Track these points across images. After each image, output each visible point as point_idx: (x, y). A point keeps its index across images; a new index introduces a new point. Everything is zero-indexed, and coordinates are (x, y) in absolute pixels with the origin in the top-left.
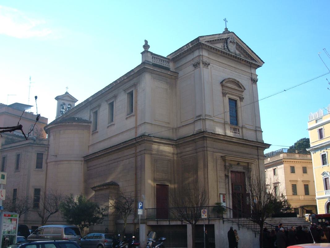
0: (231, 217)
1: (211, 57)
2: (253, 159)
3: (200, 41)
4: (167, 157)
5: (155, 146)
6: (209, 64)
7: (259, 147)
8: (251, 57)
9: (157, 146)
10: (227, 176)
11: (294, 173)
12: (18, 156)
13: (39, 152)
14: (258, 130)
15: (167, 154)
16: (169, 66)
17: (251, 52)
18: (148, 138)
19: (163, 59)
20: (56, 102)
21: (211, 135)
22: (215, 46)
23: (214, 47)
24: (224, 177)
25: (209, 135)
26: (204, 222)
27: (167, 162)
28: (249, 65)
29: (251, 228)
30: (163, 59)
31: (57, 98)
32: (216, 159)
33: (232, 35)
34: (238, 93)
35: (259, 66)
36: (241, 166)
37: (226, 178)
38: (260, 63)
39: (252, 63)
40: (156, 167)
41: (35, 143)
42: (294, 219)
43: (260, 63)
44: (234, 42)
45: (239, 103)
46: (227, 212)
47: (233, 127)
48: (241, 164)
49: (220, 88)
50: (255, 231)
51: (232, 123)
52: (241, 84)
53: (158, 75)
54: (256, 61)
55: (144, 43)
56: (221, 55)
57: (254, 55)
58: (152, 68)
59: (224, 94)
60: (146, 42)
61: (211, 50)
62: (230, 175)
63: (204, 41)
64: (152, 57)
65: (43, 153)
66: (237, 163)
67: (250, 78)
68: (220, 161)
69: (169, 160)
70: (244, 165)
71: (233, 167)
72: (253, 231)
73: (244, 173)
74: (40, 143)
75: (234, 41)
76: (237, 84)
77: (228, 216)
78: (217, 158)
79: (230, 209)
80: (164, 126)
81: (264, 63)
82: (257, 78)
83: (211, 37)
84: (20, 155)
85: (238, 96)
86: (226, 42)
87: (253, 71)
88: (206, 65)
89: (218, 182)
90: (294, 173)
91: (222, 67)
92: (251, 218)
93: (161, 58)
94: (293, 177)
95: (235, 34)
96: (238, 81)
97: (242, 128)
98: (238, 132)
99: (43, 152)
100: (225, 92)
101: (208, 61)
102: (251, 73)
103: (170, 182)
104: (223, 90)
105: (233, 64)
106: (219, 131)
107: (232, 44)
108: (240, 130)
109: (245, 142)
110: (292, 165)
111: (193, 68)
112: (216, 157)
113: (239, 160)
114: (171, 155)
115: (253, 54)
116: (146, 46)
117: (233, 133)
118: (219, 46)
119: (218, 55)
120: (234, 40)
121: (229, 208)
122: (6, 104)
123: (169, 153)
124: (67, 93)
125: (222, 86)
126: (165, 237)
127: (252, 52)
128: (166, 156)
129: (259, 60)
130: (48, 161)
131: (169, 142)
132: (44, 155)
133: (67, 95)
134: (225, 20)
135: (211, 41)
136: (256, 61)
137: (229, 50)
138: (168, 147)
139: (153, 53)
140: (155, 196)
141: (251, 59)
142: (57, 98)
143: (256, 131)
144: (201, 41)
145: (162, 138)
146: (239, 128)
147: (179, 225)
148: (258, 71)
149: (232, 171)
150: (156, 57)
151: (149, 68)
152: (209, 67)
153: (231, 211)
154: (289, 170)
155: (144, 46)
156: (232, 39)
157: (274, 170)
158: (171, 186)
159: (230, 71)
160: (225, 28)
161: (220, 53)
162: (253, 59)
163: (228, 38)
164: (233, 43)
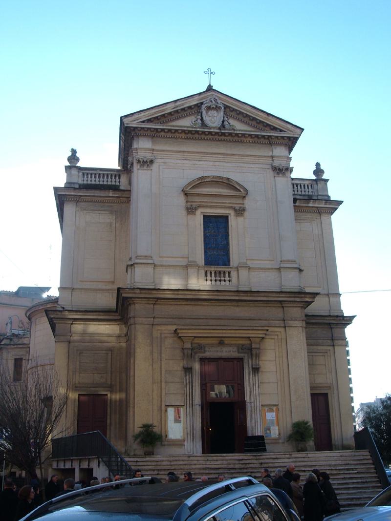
1: (157, 147)
2: (255, 328)
3: (125, 125)
4: (104, 344)
5: (78, 327)
6: (152, 162)
8: (269, 126)
9: (82, 326)
10: (188, 370)
13: (18, 357)
15: (106, 339)
16: (119, 182)
17: (265, 116)
18: (57, 314)
19: (106, 172)
21: (141, 293)
22: (171, 126)
23: (170, 128)
24: (180, 373)
25: (135, 293)
27: (104, 352)
28: (267, 141)
30: (106, 172)
32: (161, 338)
33: (213, 95)
34: (228, 202)
36: (230, 345)
37: (186, 373)
38: (291, 131)
40: (80, 363)
41: (12, 343)
42: (326, 455)
43: (291, 131)
44: (219, 105)
45: (233, 221)
47: (213, 269)
48: (227, 341)
49: (182, 199)
51: (208, 262)
52: (237, 183)
53: (91, 201)
54: (281, 131)
55: (70, 154)
56: (187, 138)
57: (274, 119)
58: (73, 194)
59: (191, 210)
60: (74, 152)
61: (154, 134)
62: (197, 366)
63: (135, 122)
64: (81, 174)
65: (22, 357)
66: (216, 341)
67: (269, 167)
68: (169, 342)
69: (111, 350)
70: (241, 342)
71: (207, 349)
73: (241, 360)
74: (18, 343)
76: (228, 183)
78: (163, 336)
80: (99, 290)
81: (303, 130)
82: (291, 166)
83: (153, 111)
84: (21, 359)
85: (231, 208)
88: (146, 165)
89: (163, 384)
91: (189, 160)
93: (100, 172)
95: (218, 91)
96: (228, 179)
97: (237, 268)
98: (223, 279)
99: (22, 355)
100: (192, 205)
101: (149, 156)
103: (111, 388)
104: (187, 202)
105: (222, 149)
106: (171, 282)
108: (234, 274)
109: (237, 296)
112: (161, 334)
113: (221, 335)
114: (113, 339)
115: (270, 118)
116: (73, 157)
117: (213, 282)
118: (186, 123)
119: (179, 140)
122: (8, 291)
123: (109, 336)
125: (186, 194)
126: (324, 492)
127: (268, 114)
128: (102, 342)
129: (289, 126)
131: (103, 315)
132: (24, 361)
135: (157, 118)
136: (281, 131)
138: (107, 326)
139: (81, 166)
140: (74, 416)
141: (272, 129)
144: (127, 124)
145: (86, 312)
146: (229, 270)
149: (203, 360)
150: (90, 172)
151: (67, 193)
152: (155, 166)
155: (70, 159)
156: (211, 101)
158: (114, 397)
159: (211, 163)
161: (183, 135)
162: (275, 129)
163: (202, 103)
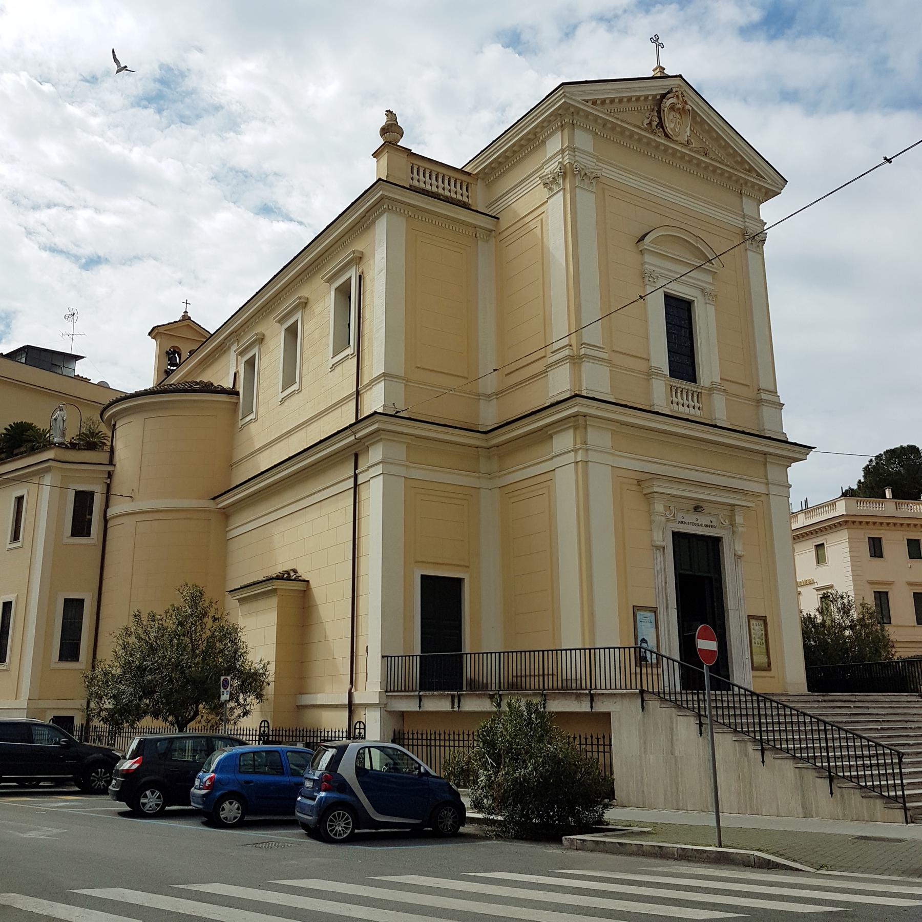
0: (678, 689)
7: (771, 454)
11: (881, 556)
12: (20, 500)
14: (766, 399)
16: (468, 197)
20: (152, 345)
26: (366, 706)
29: (690, 705)
31: (155, 332)
35: (770, 194)
39: (746, 182)
46: (660, 671)
50: (761, 740)
55: (383, 120)
72: (754, 740)
75: (684, 107)
77: (667, 684)
79: (674, 661)
86: (656, 109)
87: (748, 205)
90: (881, 556)
92: (163, 807)
94: (878, 570)
102: (744, 216)
107: (678, 116)
110: (875, 534)
111: (545, 193)
120: (686, 103)
121: (668, 658)
124: (186, 318)
130: (111, 512)
133: (187, 322)
134: (655, 40)
137: (666, 135)
142: (155, 332)
143: (759, 401)
147: (585, 713)
148: (769, 211)
153: (676, 664)
154: (865, 548)
155: (384, 131)
156: (677, 96)
157: (820, 547)
160: (656, 65)
162: (751, 169)
164: (683, 112)
